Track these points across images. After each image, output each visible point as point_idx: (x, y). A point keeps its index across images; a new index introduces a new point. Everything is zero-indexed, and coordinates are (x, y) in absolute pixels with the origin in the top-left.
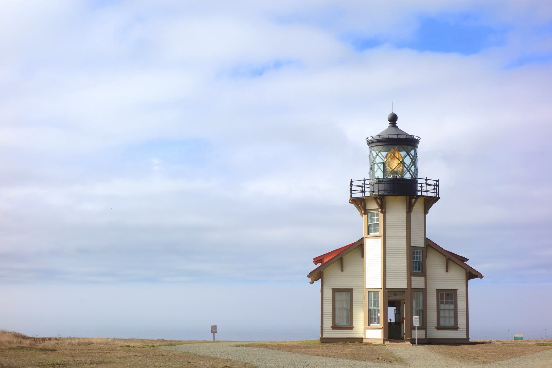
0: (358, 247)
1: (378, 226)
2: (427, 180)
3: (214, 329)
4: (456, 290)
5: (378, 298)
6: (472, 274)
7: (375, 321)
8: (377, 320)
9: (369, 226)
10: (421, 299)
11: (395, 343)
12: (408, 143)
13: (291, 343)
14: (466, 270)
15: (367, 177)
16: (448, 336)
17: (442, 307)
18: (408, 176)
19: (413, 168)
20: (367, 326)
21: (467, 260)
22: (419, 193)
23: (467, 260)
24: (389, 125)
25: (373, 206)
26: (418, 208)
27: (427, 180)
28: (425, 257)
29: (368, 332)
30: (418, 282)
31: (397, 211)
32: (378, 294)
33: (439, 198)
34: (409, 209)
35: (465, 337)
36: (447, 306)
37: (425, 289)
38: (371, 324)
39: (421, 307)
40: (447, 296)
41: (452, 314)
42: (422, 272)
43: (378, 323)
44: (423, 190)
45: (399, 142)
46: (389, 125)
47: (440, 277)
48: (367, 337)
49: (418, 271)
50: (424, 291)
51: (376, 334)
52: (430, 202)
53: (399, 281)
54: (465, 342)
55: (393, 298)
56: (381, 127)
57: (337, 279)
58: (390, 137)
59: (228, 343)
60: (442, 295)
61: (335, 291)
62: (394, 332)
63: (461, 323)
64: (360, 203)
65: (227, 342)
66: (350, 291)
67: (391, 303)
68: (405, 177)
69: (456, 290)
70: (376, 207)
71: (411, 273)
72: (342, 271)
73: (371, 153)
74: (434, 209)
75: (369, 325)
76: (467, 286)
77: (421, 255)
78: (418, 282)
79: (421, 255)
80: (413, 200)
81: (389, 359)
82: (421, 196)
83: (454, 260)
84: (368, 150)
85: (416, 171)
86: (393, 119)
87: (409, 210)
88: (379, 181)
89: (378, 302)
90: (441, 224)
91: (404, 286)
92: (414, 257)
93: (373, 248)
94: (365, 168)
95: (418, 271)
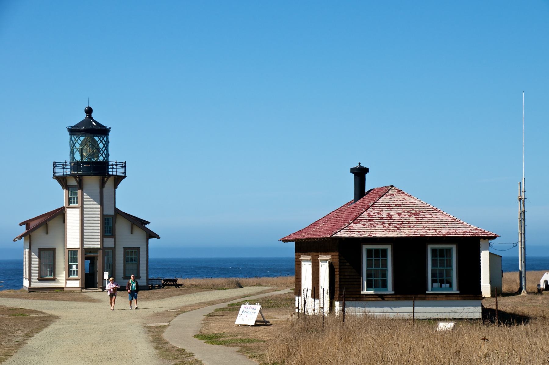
0: (61, 213)
1: (77, 199)
2: (116, 162)
4: (138, 249)
5: (77, 255)
6: (151, 235)
7: (74, 274)
8: (76, 273)
9: (70, 198)
10: (111, 256)
12: (104, 131)
15: (68, 160)
19: (105, 152)
20: (67, 278)
21: (148, 223)
23: (148, 223)
26: (109, 183)
27: (116, 162)
28: (115, 222)
29: (68, 282)
31: (92, 182)
32: (77, 251)
33: (126, 176)
34: (102, 185)
38: (71, 276)
39: (111, 263)
40: (132, 255)
42: (112, 235)
43: (77, 275)
45: (91, 131)
47: (126, 238)
48: (67, 286)
49: (109, 234)
50: (113, 249)
51: (75, 284)
52: (118, 179)
55: (89, 255)
57: (42, 240)
60: (128, 252)
61: (40, 250)
62: (90, 281)
64: (62, 180)
66: (53, 250)
67: (86, 258)
69: (138, 249)
70: (75, 183)
72: (47, 233)
73: (71, 140)
75: (69, 277)
77: (111, 221)
78: (109, 243)
79: (111, 222)
80: (106, 179)
81: (346, 329)
83: (139, 224)
84: (69, 137)
85: (107, 155)
86: (89, 111)
87: (102, 185)
89: (77, 258)
90: (126, 199)
91: (98, 245)
92: (106, 223)
93: (73, 216)
94: (63, 150)
95: (109, 234)
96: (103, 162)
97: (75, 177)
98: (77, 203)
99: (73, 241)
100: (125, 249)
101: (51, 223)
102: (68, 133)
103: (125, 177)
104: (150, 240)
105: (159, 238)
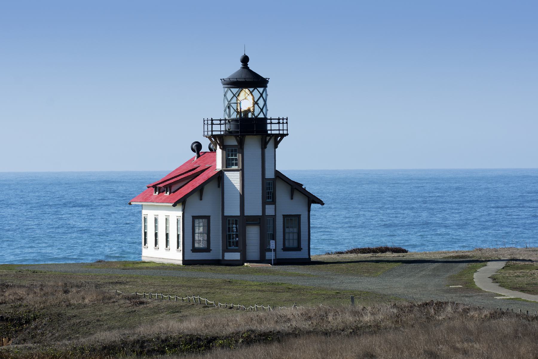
4: (299, 216)
6: (312, 199)
14: (309, 197)
17: (287, 230)
18: (261, 116)
22: (269, 132)
24: (241, 66)
25: (232, 142)
26: (270, 145)
27: (212, 120)
30: (270, 210)
31: (252, 146)
34: (264, 146)
35: (307, 257)
36: (291, 230)
37: (275, 215)
40: (293, 221)
41: (296, 236)
42: (273, 201)
44: (273, 128)
46: (241, 66)
47: (286, 206)
50: (274, 217)
52: (278, 138)
53: (254, 208)
54: (307, 262)
56: (234, 68)
58: (247, 80)
59: (389, 255)
63: (304, 244)
68: (237, 144)
69: (299, 216)
70: (235, 143)
71: (264, 204)
72: (201, 199)
74: (283, 144)
76: (309, 211)
78: (270, 210)
82: (271, 134)
83: (296, 188)
86: (245, 60)
87: (264, 146)
88: (235, 120)
90: (288, 160)
96: (252, 118)
97: (236, 137)
98: (236, 164)
99: (233, 209)
100: (284, 216)
101: (189, 200)
102: (268, 85)
103: (287, 134)
104: (313, 206)
105: (322, 204)
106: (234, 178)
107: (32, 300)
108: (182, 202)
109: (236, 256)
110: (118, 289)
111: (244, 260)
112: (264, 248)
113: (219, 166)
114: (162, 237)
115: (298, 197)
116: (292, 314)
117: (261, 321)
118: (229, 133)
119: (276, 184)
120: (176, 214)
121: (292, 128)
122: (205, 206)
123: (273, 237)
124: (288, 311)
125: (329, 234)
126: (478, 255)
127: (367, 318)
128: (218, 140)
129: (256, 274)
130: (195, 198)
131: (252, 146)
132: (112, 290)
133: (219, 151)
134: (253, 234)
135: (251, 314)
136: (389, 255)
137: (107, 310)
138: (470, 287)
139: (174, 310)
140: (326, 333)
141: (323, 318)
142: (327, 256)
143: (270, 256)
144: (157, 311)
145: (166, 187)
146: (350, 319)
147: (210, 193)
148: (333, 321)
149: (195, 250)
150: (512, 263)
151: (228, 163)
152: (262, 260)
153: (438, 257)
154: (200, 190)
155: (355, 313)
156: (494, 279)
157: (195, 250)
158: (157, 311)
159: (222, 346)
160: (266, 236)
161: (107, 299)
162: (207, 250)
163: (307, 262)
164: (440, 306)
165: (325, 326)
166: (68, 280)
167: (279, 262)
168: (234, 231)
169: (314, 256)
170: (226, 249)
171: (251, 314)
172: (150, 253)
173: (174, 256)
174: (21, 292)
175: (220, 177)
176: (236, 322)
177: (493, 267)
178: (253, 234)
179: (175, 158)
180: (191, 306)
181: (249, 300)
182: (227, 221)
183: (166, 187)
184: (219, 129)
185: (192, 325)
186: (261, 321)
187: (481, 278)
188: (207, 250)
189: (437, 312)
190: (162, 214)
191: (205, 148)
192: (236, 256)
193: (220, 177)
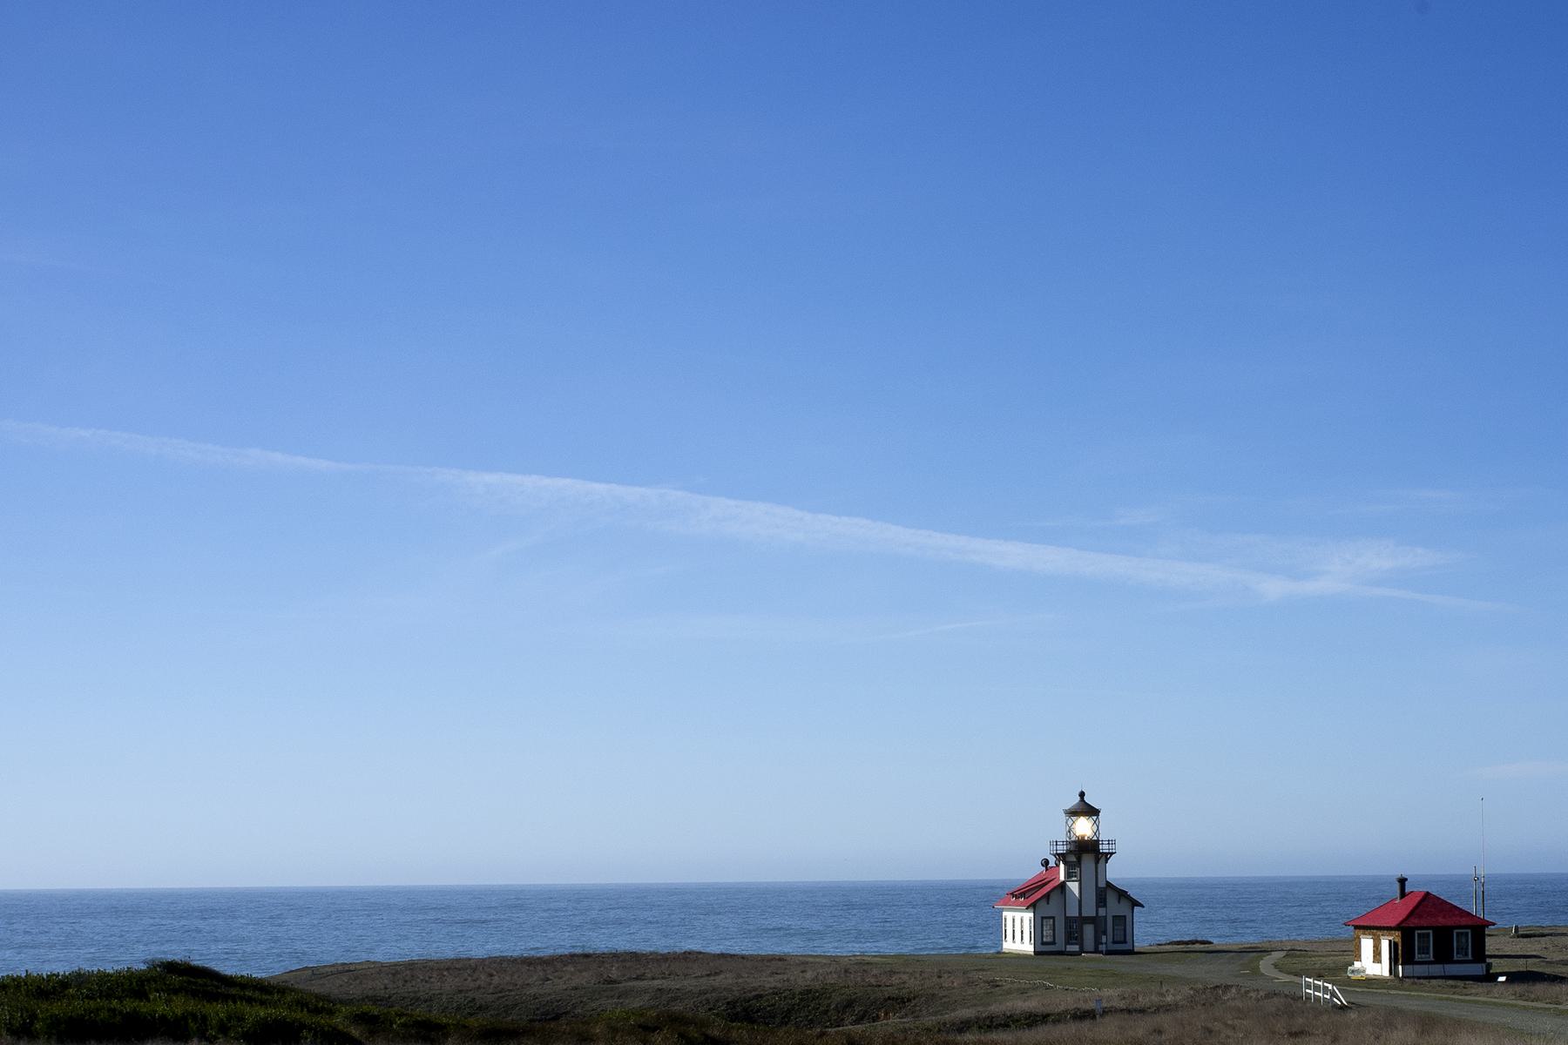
3: (1402, 881)
6: (1135, 903)
11: (830, 947)
13: (532, 953)
16: (1122, 947)
25: (1073, 859)
26: (1102, 861)
30: (1102, 912)
31: (1088, 860)
34: (1097, 862)
40: (1121, 921)
44: (1104, 848)
47: (1114, 907)
52: (1107, 856)
53: (1089, 911)
54: (1131, 952)
59: (1198, 947)
63: (1129, 938)
65: (1197, 942)
78: (1102, 912)
83: (1122, 894)
86: (1082, 795)
90: (1115, 872)
99: (1073, 912)
104: (1136, 909)
106: (1074, 887)
107: (913, 984)
108: (1033, 906)
109: (1076, 948)
110: (980, 975)
111: (1082, 951)
112: (1097, 942)
113: (1062, 878)
114: (1018, 933)
115: (1123, 901)
116: (1111, 995)
117: (1086, 1001)
118: (1069, 852)
119: (1107, 892)
120: (1028, 916)
121: (1119, 848)
122: (1052, 909)
123: (1105, 933)
124: (1107, 992)
125: (1144, 933)
126: (1266, 946)
127: (1169, 999)
128: (1061, 857)
129: (1091, 962)
130: (1043, 903)
131: (1088, 860)
132: (976, 976)
133: (1062, 866)
134: (1089, 930)
135: (1080, 995)
136: (1198, 947)
137: (970, 992)
138: (1256, 972)
139: (1023, 992)
140: (1129, 1011)
141: (1135, 998)
142: (1072, 965)
143: (1102, 948)
144: (1009, 992)
145: (1027, 895)
146: (1155, 998)
147: (1055, 898)
148: (1143, 1001)
149: (1043, 943)
150: (1292, 953)
151: (1069, 875)
152: (1096, 951)
153: (1235, 948)
154: (1047, 896)
155: (1162, 995)
156: (1276, 966)
157: (1043, 943)
158: (1009, 992)
159: (1054, 1022)
160: (1100, 931)
161: (970, 983)
162: (1053, 943)
163: (1131, 952)
164: (1227, 987)
165: (1136, 1005)
166: (942, 966)
167: (1109, 953)
168: (1073, 929)
169: (1138, 946)
170: (1067, 943)
171: (1080, 995)
172: (1009, 946)
173: (1028, 948)
174: (905, 977)
175: (1063, 886)
176: (1064, 1001)
177: (1277, 955)
178: (1089, 930)
179: (1030, 871)
180: (1035, 988)
181: (1090, 982)
182: (1068, 920)
183: (1027, 895)
184: (1062, 849)
185: (1031, 1004)
186: (1086, 1001)
187: (1265, 965)
188: (1053, 943)
189: (1224, 993)
190: (1018, 915)
191: (1052, 864)
192: (1076, 948)
193: (1063, 886)
